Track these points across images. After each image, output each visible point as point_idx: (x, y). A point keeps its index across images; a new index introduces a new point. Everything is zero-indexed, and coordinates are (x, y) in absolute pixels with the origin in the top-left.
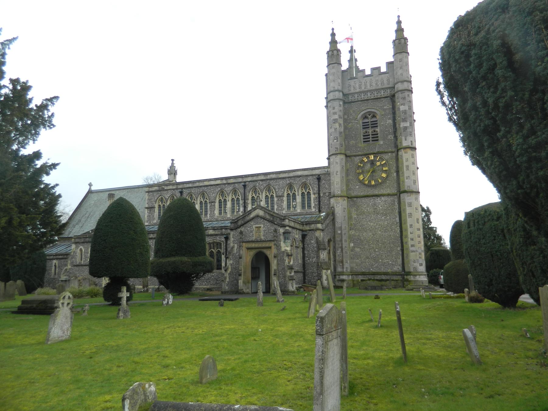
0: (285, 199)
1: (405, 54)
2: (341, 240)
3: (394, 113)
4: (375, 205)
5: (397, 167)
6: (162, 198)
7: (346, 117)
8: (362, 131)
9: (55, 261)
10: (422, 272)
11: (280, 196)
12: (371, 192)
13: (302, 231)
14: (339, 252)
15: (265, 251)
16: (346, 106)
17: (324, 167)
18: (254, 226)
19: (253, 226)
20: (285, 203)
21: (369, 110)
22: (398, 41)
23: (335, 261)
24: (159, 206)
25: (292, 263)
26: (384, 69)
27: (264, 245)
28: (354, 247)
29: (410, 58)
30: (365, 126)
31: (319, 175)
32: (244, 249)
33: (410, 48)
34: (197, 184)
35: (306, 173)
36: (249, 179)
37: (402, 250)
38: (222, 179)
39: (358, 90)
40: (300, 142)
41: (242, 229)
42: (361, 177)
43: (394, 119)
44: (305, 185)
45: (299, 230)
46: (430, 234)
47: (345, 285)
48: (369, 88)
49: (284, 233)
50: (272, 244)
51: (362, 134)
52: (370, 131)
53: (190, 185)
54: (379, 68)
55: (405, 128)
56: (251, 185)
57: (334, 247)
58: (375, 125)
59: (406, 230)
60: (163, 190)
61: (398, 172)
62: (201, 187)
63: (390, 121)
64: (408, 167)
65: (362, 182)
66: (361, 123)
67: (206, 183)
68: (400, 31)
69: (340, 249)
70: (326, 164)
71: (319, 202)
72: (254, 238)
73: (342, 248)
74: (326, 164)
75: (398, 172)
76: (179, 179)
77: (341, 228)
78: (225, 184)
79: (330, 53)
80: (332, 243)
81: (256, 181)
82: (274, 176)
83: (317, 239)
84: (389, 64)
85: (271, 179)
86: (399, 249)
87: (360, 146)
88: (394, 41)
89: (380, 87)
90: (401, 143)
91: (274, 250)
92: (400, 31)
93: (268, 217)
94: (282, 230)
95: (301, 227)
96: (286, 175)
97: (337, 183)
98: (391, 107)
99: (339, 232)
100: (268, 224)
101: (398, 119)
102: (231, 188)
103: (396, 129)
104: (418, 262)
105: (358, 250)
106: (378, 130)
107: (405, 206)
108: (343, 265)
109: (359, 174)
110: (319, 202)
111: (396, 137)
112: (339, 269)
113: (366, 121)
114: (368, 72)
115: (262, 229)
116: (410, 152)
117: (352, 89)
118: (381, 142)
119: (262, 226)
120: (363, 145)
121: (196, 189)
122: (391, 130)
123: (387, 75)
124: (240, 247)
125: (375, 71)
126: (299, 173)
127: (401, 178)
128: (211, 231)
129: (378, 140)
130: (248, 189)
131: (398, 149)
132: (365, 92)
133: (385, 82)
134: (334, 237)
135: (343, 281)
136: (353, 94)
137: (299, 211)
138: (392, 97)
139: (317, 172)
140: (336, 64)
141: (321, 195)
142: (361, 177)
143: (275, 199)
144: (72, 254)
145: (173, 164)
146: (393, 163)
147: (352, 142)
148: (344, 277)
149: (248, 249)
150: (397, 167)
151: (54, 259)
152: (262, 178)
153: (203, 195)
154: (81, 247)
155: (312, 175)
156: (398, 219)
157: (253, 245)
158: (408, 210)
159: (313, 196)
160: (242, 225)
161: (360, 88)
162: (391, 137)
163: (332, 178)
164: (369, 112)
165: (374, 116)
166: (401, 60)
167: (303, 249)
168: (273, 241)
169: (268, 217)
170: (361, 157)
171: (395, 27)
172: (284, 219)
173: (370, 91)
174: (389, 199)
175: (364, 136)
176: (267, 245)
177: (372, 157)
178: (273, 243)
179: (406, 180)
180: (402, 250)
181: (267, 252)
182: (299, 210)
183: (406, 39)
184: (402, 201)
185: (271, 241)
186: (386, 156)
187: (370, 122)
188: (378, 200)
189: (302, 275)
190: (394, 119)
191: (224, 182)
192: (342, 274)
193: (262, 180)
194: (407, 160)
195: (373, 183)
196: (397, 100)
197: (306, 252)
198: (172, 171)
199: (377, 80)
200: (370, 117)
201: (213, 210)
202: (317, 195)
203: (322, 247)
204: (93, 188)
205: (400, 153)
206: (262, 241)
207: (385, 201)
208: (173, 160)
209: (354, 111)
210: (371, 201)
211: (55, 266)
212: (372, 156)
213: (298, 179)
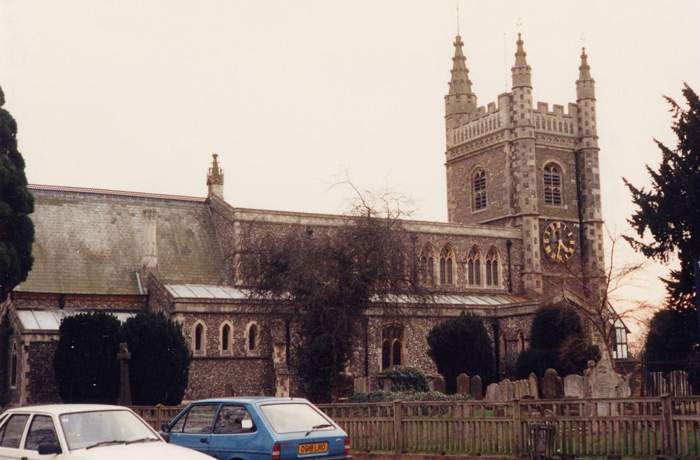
33: (534, 81)
54: (561, 108)
122: (575, 194)
145: (215, 164)
198: (215, 178)
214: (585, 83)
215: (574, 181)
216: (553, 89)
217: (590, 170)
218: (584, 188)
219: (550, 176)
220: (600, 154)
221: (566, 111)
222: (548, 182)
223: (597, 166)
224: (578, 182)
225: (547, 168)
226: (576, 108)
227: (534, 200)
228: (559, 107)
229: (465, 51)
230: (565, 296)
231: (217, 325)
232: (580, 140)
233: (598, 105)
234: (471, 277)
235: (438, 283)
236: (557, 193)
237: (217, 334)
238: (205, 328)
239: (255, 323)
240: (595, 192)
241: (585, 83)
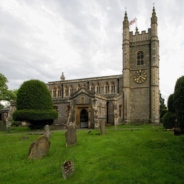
0: (105, 88)
1: (156, 24)
2: (126, 106)
3: (150, 52)
4: (140, 91)
5: (150, 75)
7: (131, 53)
8: (137, 60)
9: (5, 113)
10: (157, 119)
11: (103, 87)
12: (139, 86)
13: (107, 101)
14: (125, 110)
15: (86, 109)
16: (131, 48)
17: (121, 75)
18: (81, 97)
19: (80, 97)
20: (105, 90)
21: (140, 50)
22: (153, 18)
23: (123, 114)
24: (54, 91)
25: (97, 114)
26: (140, 33)
27: (85, 106)
28: (131, 109)
29: (160, 62)
30: (138, 58)
31: (118, 78)
32: (76, 108)
34: (69, 82)
35: (114, 77)
36: (90, 80)
37: (150, 110)
38: (79, 80)
39: (136, 41)
40: (109, 63)
41: (75, 99)
42: (136, 80)
43: (150, 55)
44: (113, 83)
45: (106, 100)
46: (162, 101)
47: (127, 123)
48: (140, 40)
49: (94, 100)
50: (88, 106)
51: (137, 61)
52: (140, 60)
54: (145, 31)
55: (154, 58)
56: (90, 83)
57: (123, 109)
58: (142, 57)
59: (152, 102)
60: (55, 84)
61: (150, 78)
62: (70, 83)
63: (148, 55)
64: (154, 75)
65: (136, 82)
66: (137, 56)
69: (125, 109)
70: (122, 74)
71: (118, 90)
72: (81, 103)
73: (126, 109)
74: (122, 74)
75: (150, 78)
76: (66, 79)
77: (126, 101)
79: (124, 22)
80: (122, 107)
81: (93, 81)
82: (100, 79)
83: (113, 104)
85: (99, 80)
86: (149, 109)
87: (136, 66)
89: (145, 39)
90: (152, 64)
91: (90, 109)
93: (87, 93)
94: (93, 99)
95: (106, 99)
96: (105, 78)
97: (126, 82)
98: (149, 49)
99: (126, 102)
100: (87, 96)
101: (152, 54)
103: (151, 59)
104: (156, 115)
105: (133, 110)
107: (152, 92)
108: (126, 115)
109: (135, 78)
110: (118, 90)
111: (150, 62)
112: (125, 117)
113: (139, 55)
115: (84, 99)
116: (156, 68)
117: (134, 40)
118: (145, 65)
119: (84, 97)
120: (137, 66)
122: (149, 59)
123: (148, 34)
124: (74, 107)
125: (143, 32)
126: (111, 77)
127: (151, 80)
128: (69, 101)
129: (143, 64)
131: (151, 67)
132: (139, 42)
133: (147, 37)
134: (123, 105)
135: (126, 122)
136: (134, 43)
137: (110, 93)
138: (150, 45)
139: (118, 77)
140: (127, 28)
141: (119, 87)
142: (136, 80)
143: (101, 89)
144: (10, 110)
146: (148, 74)
147: (133, 64)
148: (127, 121)
149: (78, 108)
150: (150, 75)
151: (5, 112)
152: (96, 79)
153: (72, 86)
154: (14, 107)
155: (116, 78)
156: (149, 97)
157: (80, 106)
158: (153, 93)
159: (116, 87)
160: (76, 97)
161: (137, 40)
162: (148, 62)
163: (123, 80)
164: (140, 51)
165: (142, 53)
166: (154, 27)
167: (107, 109)
168: (89, 104)
169: (87, 93)
170: (136, 71)
171: (152, 12)
172: (94, 94)
173: (141, 41)
174: (146, 89)
175: (138, 62)
176: (86, 106)
177: (140, 71)
178: (89, 105)
179: (153, 81)
180: (150, 110)
181: (87, 109)
182: (110, 93)
183: (156, 17)
184: (151, 90)
185: (88, 104)
186: (146, 71)
187: (141, 55)
188: (142, 90)
189: (106, 120)
190: (150, 55)
191: (80, 81)
192: (126, 119)
194: (154, 72)
195: (140, 82)
196: (151, 45)
197: (108, 110)
199: (144, 37)
200: (140, 53)
202: (117, 87)
203: (115, 108)
205: (151, 69)
206: (84, 104)
207: (145, 90)
208: (63, 73)
209: (134, 51)
210: (139, 90)
211: (6, 115)
212: (140, 71)
213: (110, 80)
214: (154, 20)
216: (142, 25)
228: (144, 32)
241: (154, 20)
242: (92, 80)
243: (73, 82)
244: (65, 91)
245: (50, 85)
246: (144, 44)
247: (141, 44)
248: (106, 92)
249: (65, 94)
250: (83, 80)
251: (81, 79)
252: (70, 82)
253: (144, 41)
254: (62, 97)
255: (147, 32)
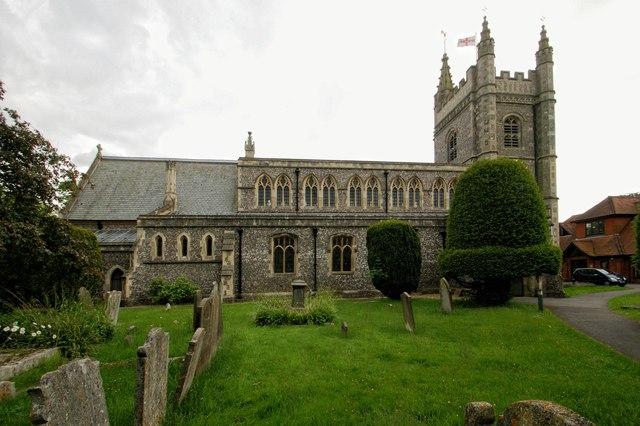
6: (264, 177)
26: (512, 76)
33: (497, 50)
34: (320, 165)
36: (391, 167)
38: (355, 162)
48: (513, 91)
53: (310, 165)
54: (522, 74)
62: (326, 169)
67: (334, 165)
68: (544, 41)
76: (257, 155)
78: (359, 169)
81: (313, 168)
82: (420, 168)
84: (531, 72)
85: (417, 171)
88: (537, 53)
92: (544, 41)
102: (307, 172)
106: (519, 135)
114: (512, 76)
118: (523, 148)
121: (319, 171)
122: (532, 138)
130: (389, 178)
132: (511, 95)
138: (535, 108)
143: (337, 194)
144: (141, 243)
145: (250, 138)
152: (407, 168)
159: (380, 192)
166: (485, 63)
171: (539, 38)
183: (551, 48)
191: (359, 166)
193: (407, 171)
198: (250, 148)
201: (343, 201)
204: (104, 153)
208: (250, 133)
214: (544, 54)
215: (532, 129)
216: (514, 59)
217: (546, 118)
218: (540, 133)
219: (511, 127)
220: (556, 106)
221: (526, 76)
222: (507, 130)
223: (553, 114)
224: (535, 129)
225: (507, 121)
226: (534, 74)
227: (493, 142)
228: (519, 75)
229: (449, 63)
230: (519, 157)
231: (174, 237)
232: (538, 96)
233: (556, 69)
234: (436, 202)
235: (407, 206)
236: (515, 140)
237: (175, 243)
238: (164, 239)
239: (209, 234)
240: (550, 134)
241: (544, 54)
242: (398, 167)
243: (334, 168)
244: (304, 192)
245: (247, 166)
246: (520, 101)
247: (514, 100)
248: (261, 203)
249: (303, 202)
250: (368, 166)
251: (362, 163)
252: (326, 166)
253: (522, 96)
254: (297, 210)
255: (526, 76)
